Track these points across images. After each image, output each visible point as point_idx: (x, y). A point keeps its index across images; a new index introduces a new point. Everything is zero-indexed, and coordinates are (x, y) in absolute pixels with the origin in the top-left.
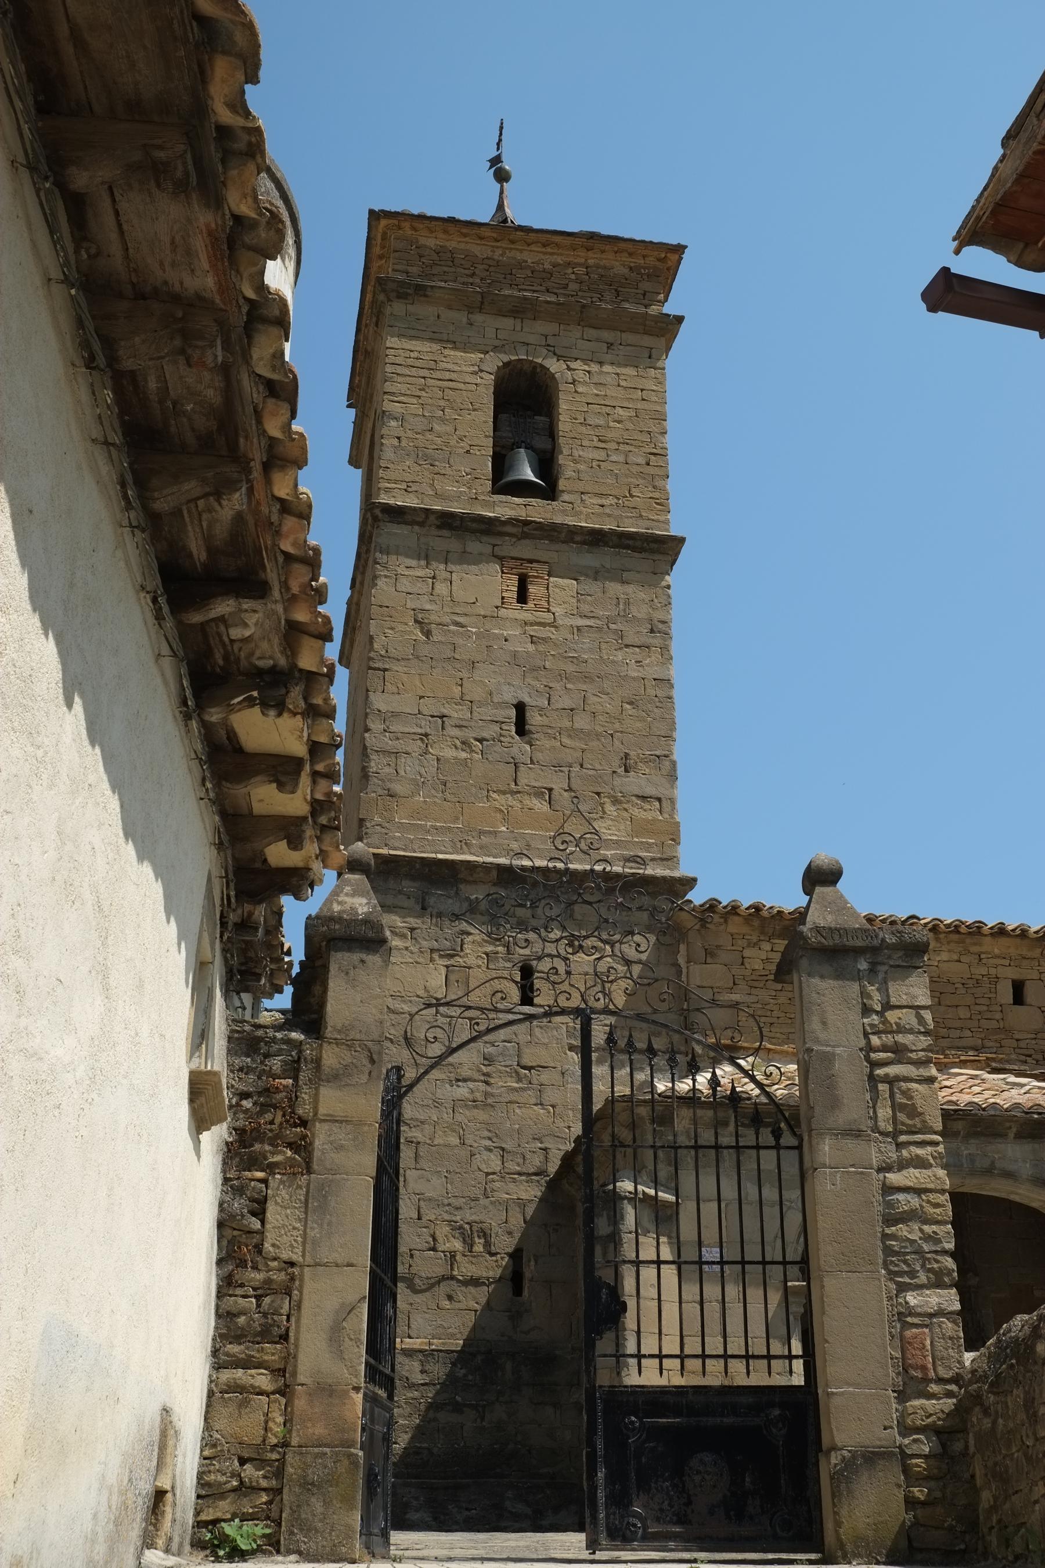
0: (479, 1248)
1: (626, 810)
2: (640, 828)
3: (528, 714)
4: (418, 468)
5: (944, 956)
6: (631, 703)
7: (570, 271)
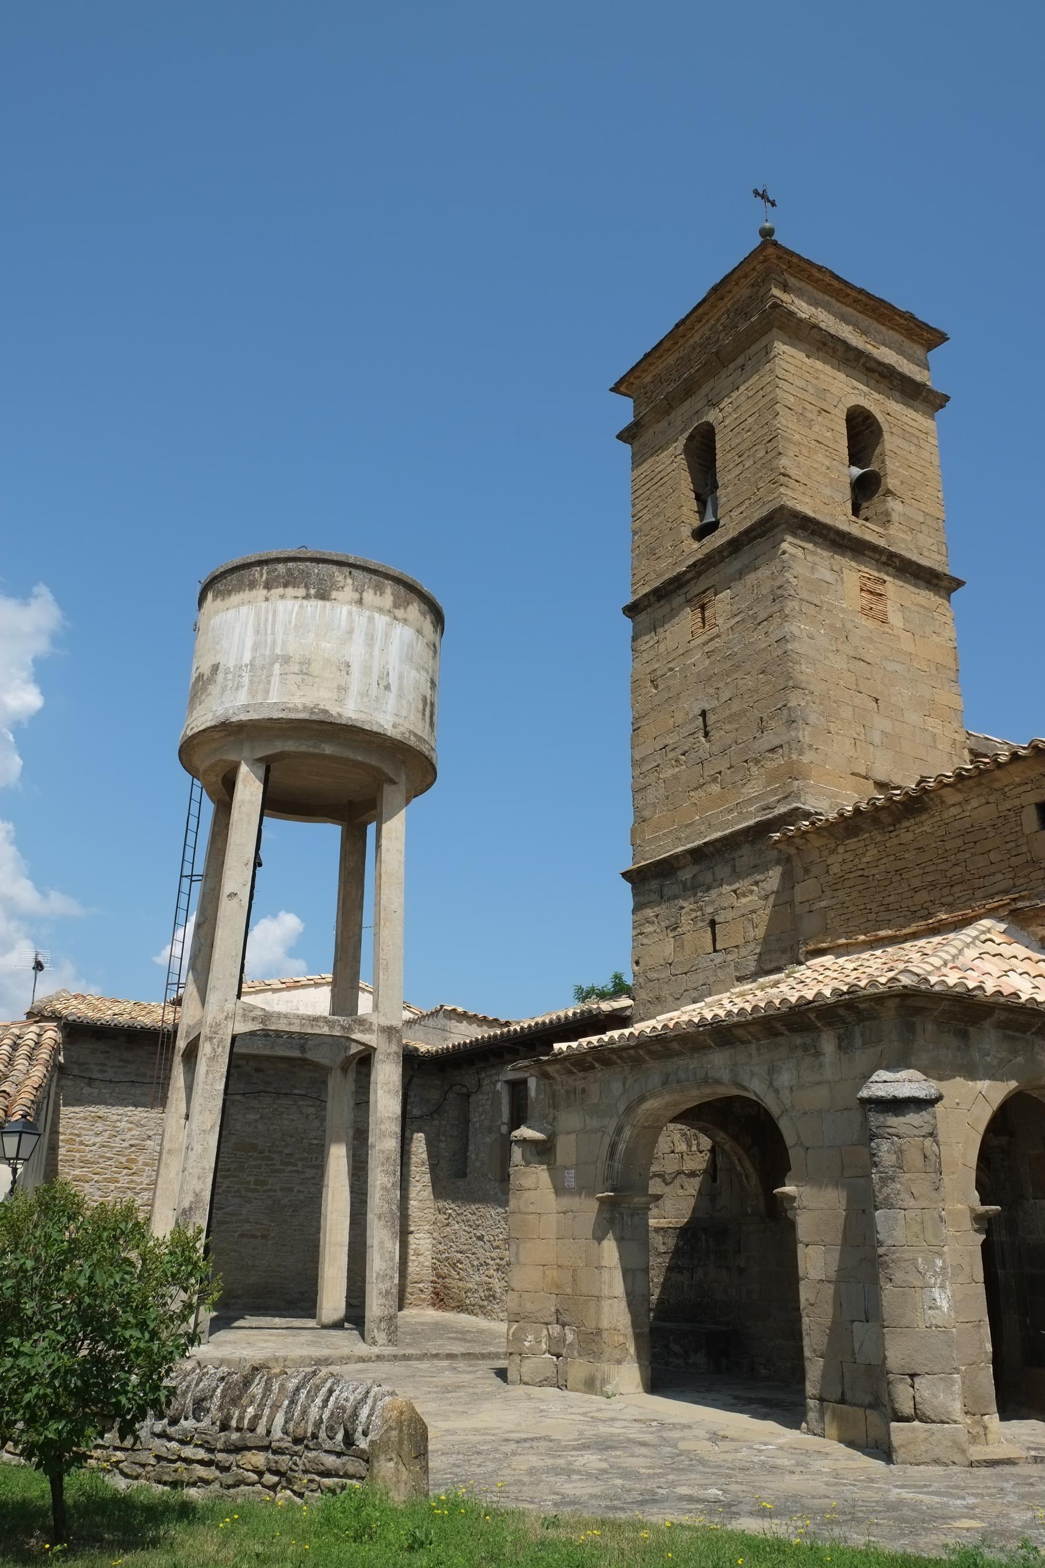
0: (694, 1148)
5: (974, 803)
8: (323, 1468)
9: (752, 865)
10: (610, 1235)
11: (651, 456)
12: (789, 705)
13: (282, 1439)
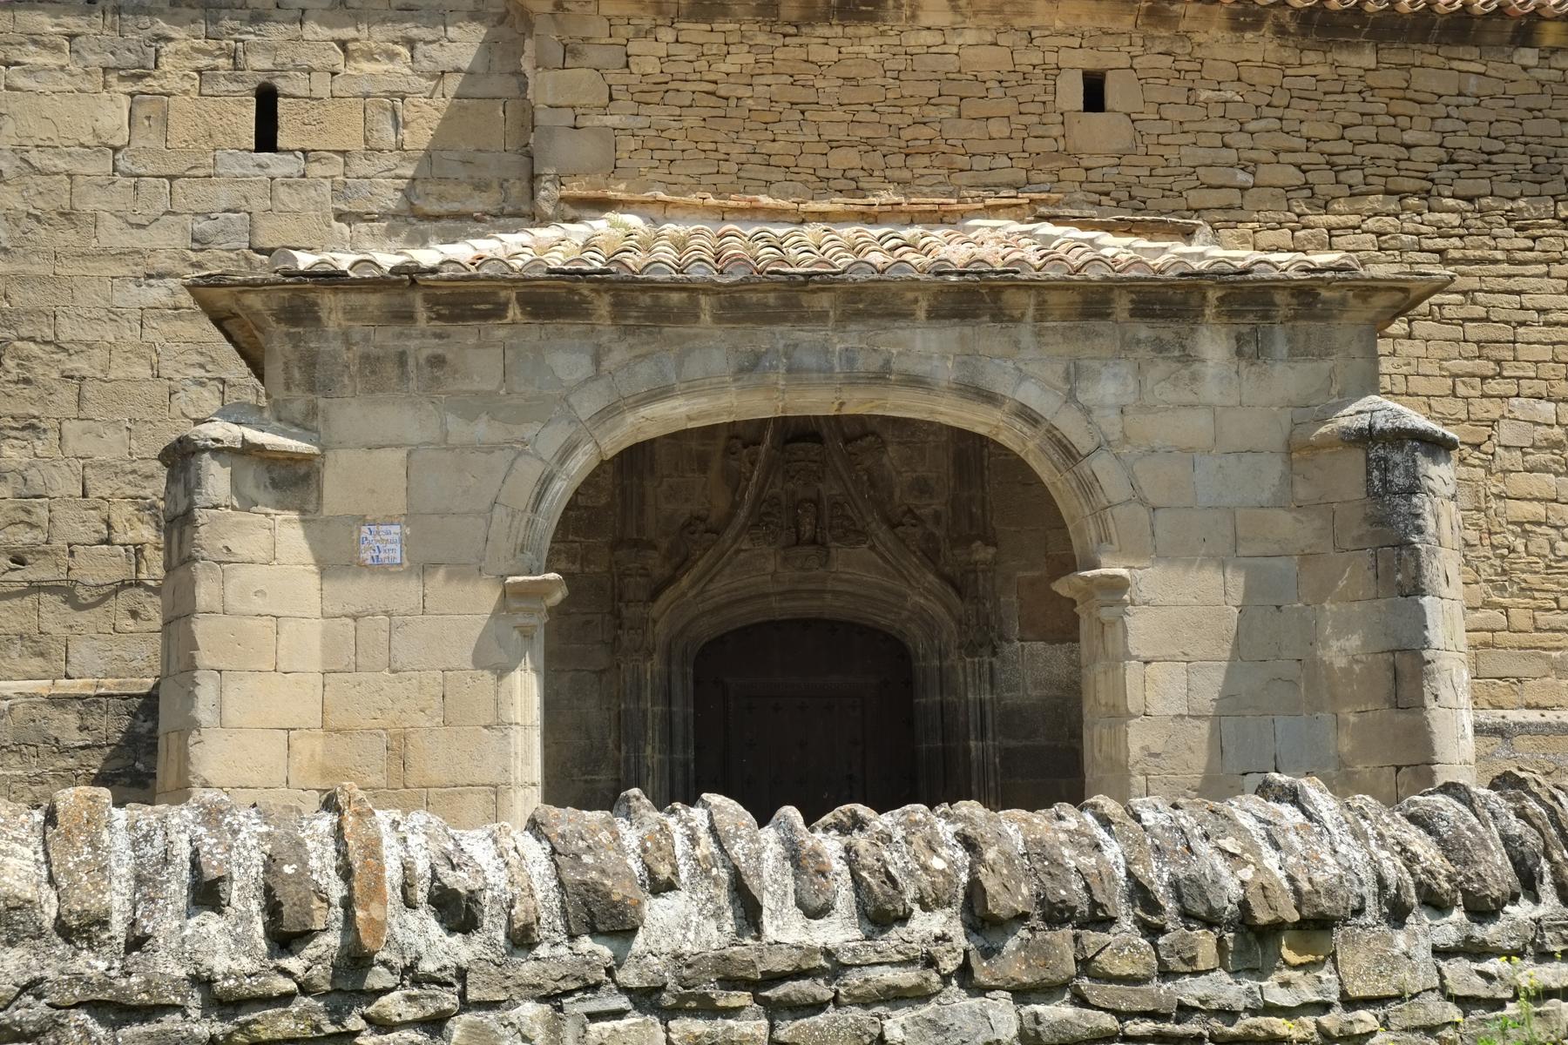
5: (970, 37)
10: (527, 662)
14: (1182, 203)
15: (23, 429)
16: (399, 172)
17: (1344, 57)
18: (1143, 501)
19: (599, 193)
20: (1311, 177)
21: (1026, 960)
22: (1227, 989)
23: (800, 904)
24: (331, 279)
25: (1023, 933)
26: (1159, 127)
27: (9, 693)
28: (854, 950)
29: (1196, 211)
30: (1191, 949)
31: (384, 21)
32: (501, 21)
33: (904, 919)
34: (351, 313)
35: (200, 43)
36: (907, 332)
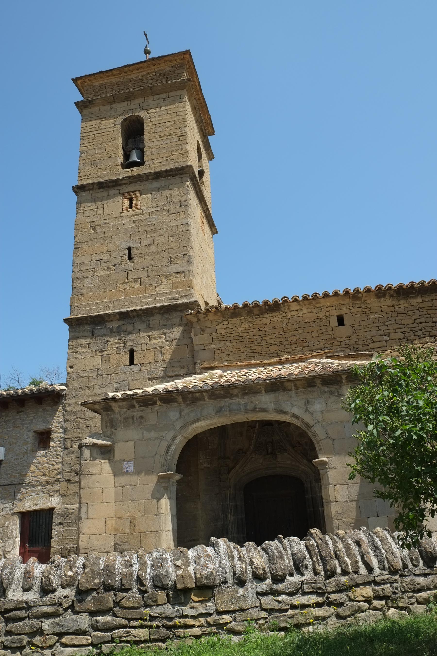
1: (170, 279)
2: (176, 285)
3: (132, 251)
4: (92, 169)
5: (305, 311)
6: (172, 236)
7: (149, 76)
8: (418, 586)
9: (161, 324)
11: (97, 119)
12: (189, 254)
13: (381, 574)
14: (369, 347)
15: (78, 440)
16: (163, 366)
17: (412, 300)
18: (330, 438)
19: (210, 366)
20: (406, 335)
21: (94, 603)
22: (169, 610)
23: (22, 588)
24: (113, 399)
25: (94, 594)
26: (360, 327)
27: (74, 508)
28: (34, 601)
29: (373, 349)
30: (155, 597)
31: (158, 329)
32: (186, 325)
33: (54, 591)
34: (120, 407)
35: (117, 341)
36: (260, 397)
